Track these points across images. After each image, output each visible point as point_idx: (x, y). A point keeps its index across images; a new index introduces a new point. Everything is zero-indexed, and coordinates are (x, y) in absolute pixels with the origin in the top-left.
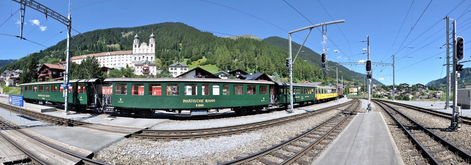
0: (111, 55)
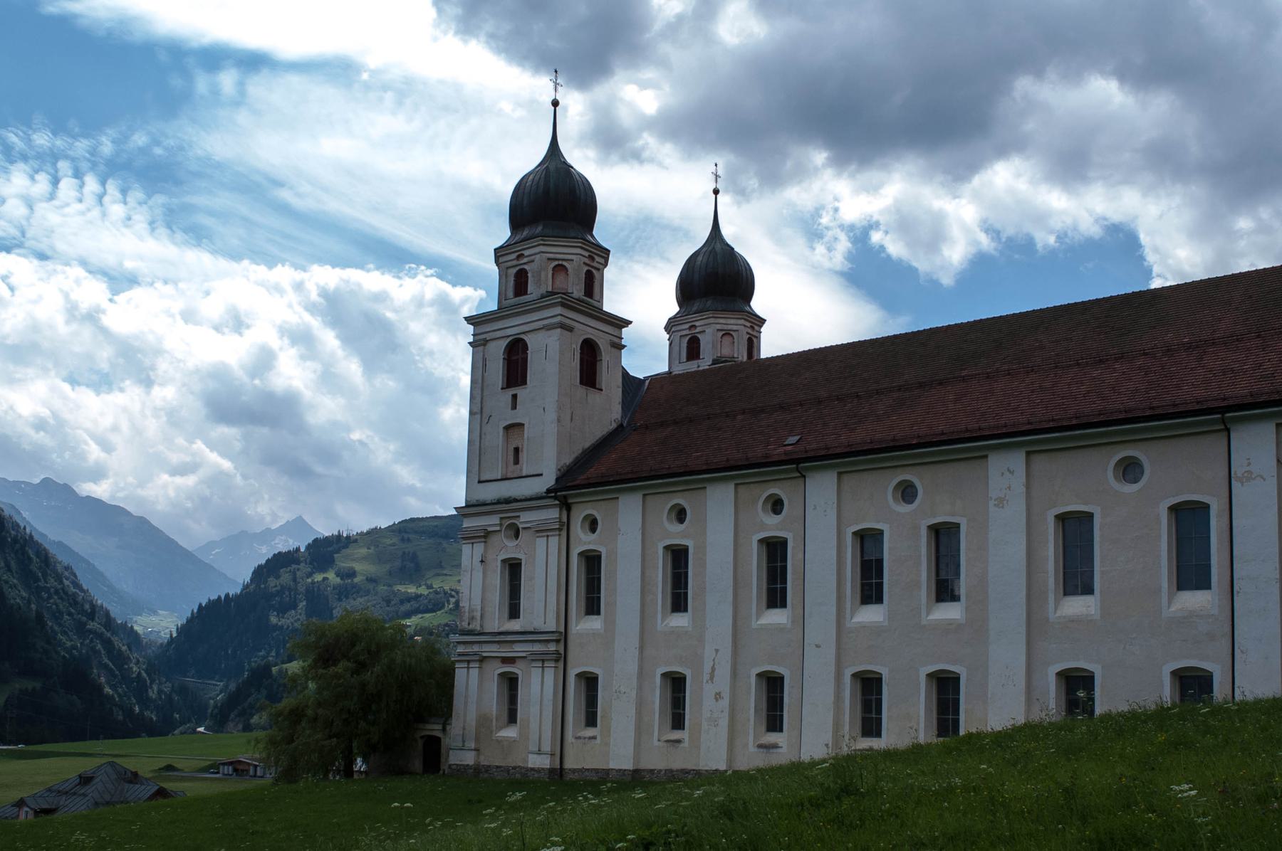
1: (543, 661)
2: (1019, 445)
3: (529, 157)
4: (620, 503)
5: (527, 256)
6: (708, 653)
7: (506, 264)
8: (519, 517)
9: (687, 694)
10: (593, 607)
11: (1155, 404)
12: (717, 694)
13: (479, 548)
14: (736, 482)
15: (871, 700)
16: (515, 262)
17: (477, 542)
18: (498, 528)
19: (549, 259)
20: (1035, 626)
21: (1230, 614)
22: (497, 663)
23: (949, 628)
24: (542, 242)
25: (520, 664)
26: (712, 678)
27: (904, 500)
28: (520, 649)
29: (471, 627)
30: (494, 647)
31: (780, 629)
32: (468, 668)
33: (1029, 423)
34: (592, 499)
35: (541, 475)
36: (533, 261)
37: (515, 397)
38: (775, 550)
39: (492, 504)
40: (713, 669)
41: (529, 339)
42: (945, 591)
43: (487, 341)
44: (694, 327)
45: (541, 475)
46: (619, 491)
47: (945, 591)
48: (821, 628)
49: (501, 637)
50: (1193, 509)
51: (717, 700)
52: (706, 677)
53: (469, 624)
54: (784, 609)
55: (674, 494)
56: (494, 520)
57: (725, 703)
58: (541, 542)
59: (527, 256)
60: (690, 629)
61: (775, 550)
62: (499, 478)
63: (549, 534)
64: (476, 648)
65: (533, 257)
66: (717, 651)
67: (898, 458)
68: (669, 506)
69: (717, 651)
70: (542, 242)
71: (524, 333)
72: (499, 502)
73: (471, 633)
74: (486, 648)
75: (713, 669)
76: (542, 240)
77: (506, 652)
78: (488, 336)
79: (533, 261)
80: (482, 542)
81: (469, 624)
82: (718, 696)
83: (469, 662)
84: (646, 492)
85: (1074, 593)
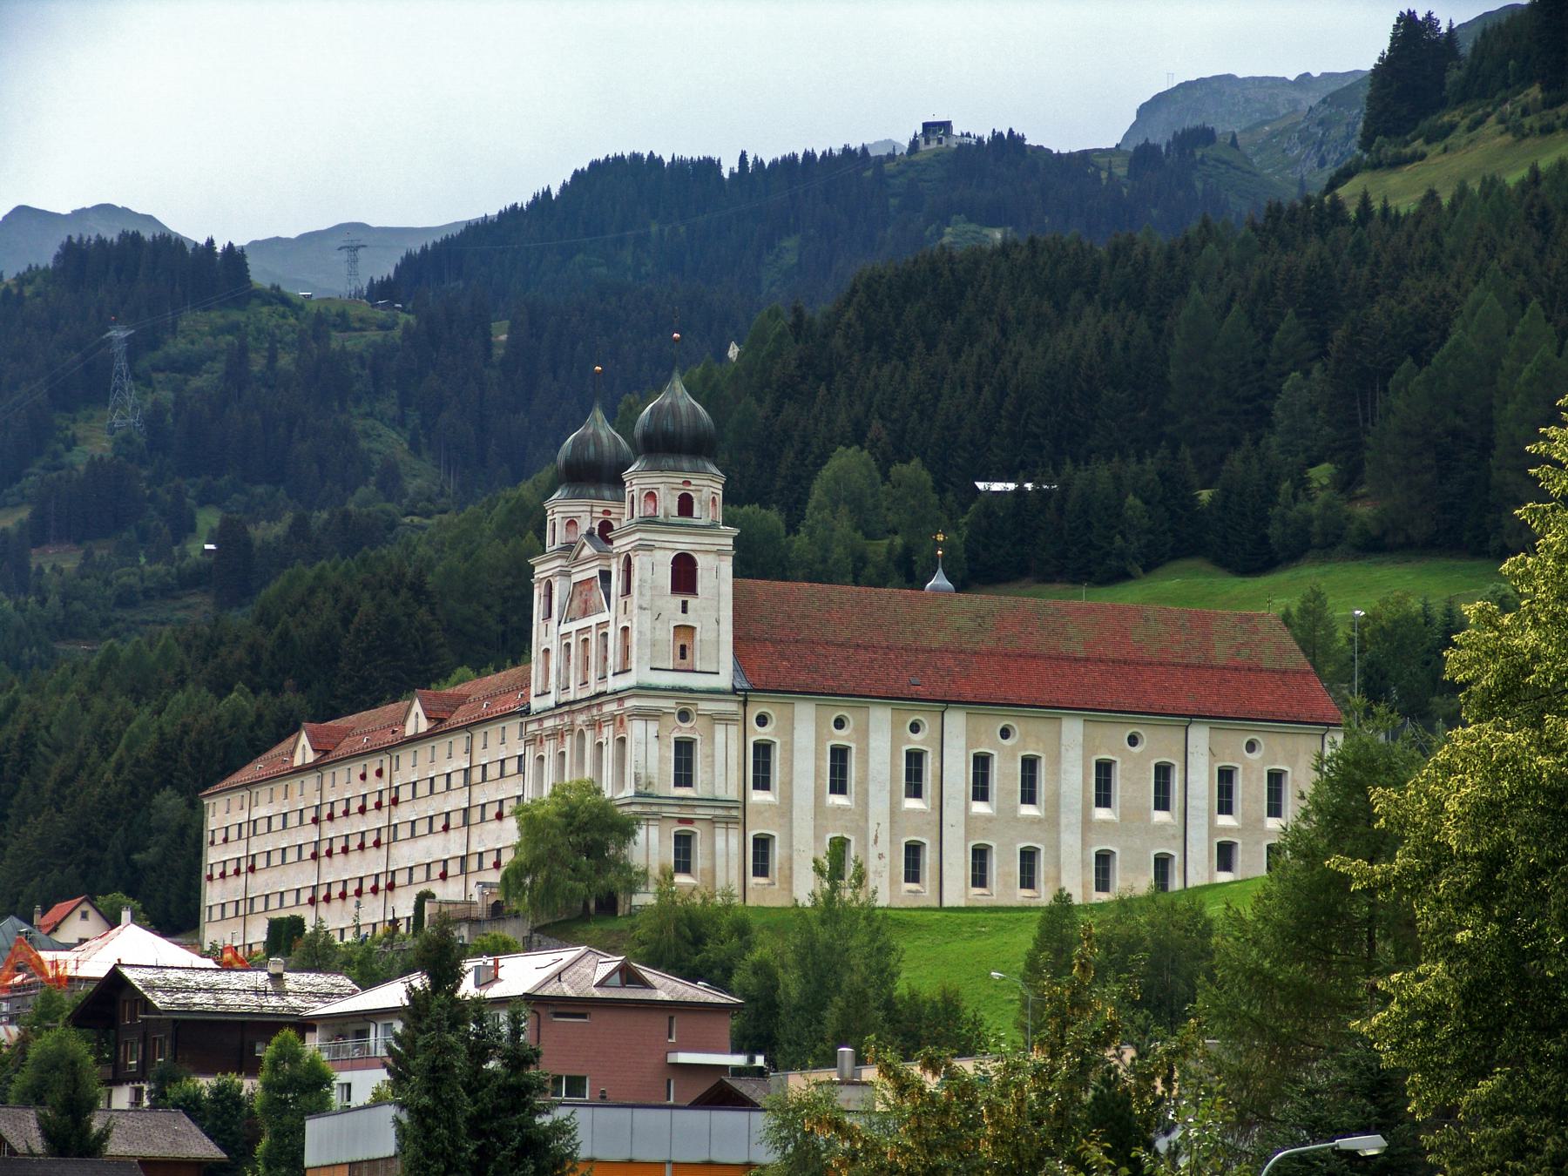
0: (439, 728)
1: (727, 823)
6: (872, 825)
9: (1266, 802)
16: (681, 486)
20: (1087, 823)
21: (938, 886)
22: (675, 822)
23: (1033, 821)
25: (697, 824)
28: (701, 813)
29: (648, 791)
30: (676, 809)
31: (922, 812)
32: (727, 828)
35: (651, 669)
36: (700, 491)
37: (685, 604)
39: (665, 690)
40: (876, 837)
41: (699, 558)
42: (1029, 797)
44: (689, 483)
45: (651, 669)
47: (1029, 797)
48: (1070, 819)
52: (871, 842)
56: (671, 703)
57: (887, 860)
64: (655, 809)
66: (879, 824)
69: (879, 824)
72: (673, 689)
73: (649, 796)
74: (665, 809)
75: (876, 837)
79: (700, 491)
82: (881, 856)
85: (911, 797)
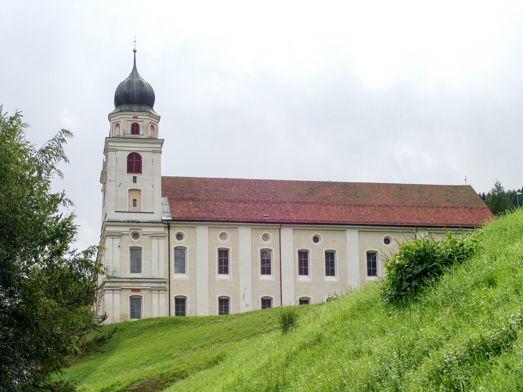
1: (159, 290)
2: (250, 225)
3: (124, 75)
4: (347, 233)
5: (139, 118)
7: (127, 119)
8: (141, 229)
10: (181, 269)
11: (273, 219)
12: (246, 304)
13: (117, 241)
14: (252, 227)
15: (222, 307)
16: (132, 119)
17: (115, 238)
18: (128, 233)
19: (150, 122)
22: (130, 291)
23: (332, 284)
24: (149, 115)
25: (142, 291)
26: (244, 298)
27: (133, 237)
30: (130, 284)
33: (388, 223)
34: (182, 226)
38: (223, 254)
40: (244, 295)
43: (117, 150)
46: (240, 225)
49: (132, 280)
50: (136, 249)
51: (247, 307)
52: (241, 298)
53: (113, 274)
54: (227, 275)
55: (384, 233)
56: (127, 229)
58: (155, 241)
59: (139, 118)
60: (231, 280)
61: (223, 254)
62: (128, 211)
63: (113, 237)
65: (143, 120)
66: (245, 288)
67: (391, 229)
68: (263, 234)
69: (245, 288)
70: (149, 115)
71: (139, 151)
72: (128, 222)
74: (123, 284)
75: (244, 295)
76: (149, 114)
77: (136, 286)
78: (118, 148)
80: (163, 239)
81: (113, 274)
83: (113, 290)
84: (210, 226)
